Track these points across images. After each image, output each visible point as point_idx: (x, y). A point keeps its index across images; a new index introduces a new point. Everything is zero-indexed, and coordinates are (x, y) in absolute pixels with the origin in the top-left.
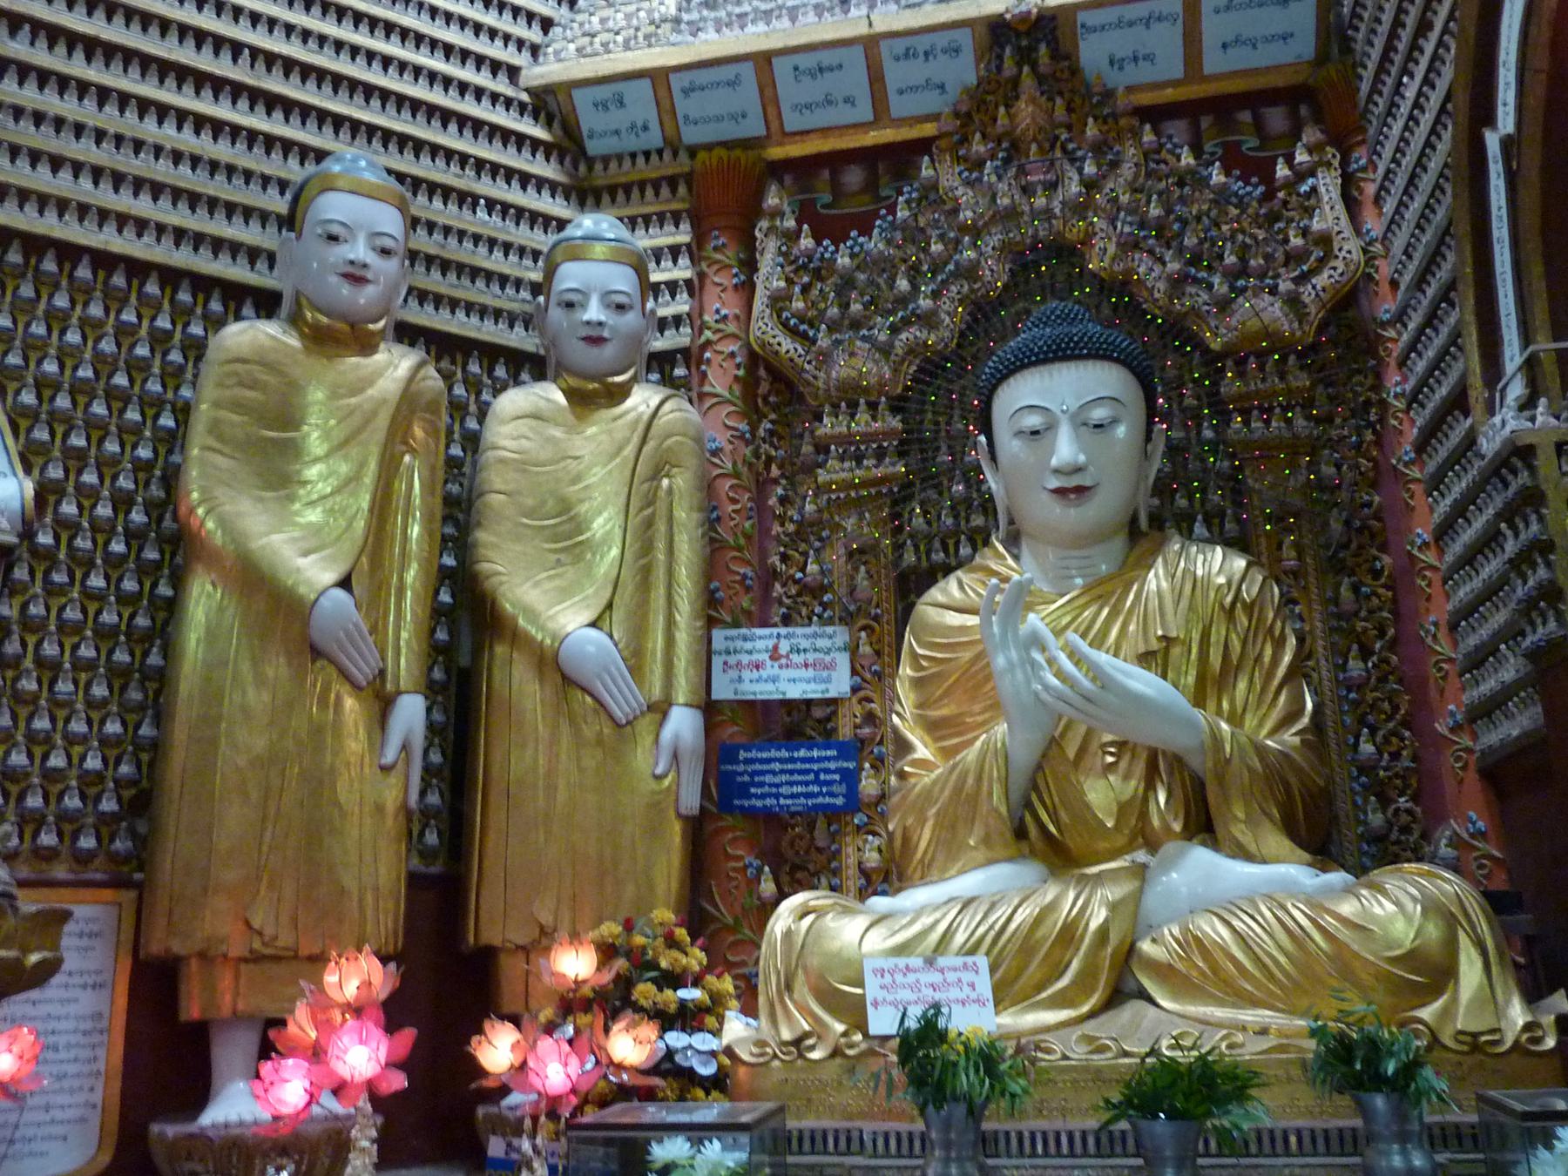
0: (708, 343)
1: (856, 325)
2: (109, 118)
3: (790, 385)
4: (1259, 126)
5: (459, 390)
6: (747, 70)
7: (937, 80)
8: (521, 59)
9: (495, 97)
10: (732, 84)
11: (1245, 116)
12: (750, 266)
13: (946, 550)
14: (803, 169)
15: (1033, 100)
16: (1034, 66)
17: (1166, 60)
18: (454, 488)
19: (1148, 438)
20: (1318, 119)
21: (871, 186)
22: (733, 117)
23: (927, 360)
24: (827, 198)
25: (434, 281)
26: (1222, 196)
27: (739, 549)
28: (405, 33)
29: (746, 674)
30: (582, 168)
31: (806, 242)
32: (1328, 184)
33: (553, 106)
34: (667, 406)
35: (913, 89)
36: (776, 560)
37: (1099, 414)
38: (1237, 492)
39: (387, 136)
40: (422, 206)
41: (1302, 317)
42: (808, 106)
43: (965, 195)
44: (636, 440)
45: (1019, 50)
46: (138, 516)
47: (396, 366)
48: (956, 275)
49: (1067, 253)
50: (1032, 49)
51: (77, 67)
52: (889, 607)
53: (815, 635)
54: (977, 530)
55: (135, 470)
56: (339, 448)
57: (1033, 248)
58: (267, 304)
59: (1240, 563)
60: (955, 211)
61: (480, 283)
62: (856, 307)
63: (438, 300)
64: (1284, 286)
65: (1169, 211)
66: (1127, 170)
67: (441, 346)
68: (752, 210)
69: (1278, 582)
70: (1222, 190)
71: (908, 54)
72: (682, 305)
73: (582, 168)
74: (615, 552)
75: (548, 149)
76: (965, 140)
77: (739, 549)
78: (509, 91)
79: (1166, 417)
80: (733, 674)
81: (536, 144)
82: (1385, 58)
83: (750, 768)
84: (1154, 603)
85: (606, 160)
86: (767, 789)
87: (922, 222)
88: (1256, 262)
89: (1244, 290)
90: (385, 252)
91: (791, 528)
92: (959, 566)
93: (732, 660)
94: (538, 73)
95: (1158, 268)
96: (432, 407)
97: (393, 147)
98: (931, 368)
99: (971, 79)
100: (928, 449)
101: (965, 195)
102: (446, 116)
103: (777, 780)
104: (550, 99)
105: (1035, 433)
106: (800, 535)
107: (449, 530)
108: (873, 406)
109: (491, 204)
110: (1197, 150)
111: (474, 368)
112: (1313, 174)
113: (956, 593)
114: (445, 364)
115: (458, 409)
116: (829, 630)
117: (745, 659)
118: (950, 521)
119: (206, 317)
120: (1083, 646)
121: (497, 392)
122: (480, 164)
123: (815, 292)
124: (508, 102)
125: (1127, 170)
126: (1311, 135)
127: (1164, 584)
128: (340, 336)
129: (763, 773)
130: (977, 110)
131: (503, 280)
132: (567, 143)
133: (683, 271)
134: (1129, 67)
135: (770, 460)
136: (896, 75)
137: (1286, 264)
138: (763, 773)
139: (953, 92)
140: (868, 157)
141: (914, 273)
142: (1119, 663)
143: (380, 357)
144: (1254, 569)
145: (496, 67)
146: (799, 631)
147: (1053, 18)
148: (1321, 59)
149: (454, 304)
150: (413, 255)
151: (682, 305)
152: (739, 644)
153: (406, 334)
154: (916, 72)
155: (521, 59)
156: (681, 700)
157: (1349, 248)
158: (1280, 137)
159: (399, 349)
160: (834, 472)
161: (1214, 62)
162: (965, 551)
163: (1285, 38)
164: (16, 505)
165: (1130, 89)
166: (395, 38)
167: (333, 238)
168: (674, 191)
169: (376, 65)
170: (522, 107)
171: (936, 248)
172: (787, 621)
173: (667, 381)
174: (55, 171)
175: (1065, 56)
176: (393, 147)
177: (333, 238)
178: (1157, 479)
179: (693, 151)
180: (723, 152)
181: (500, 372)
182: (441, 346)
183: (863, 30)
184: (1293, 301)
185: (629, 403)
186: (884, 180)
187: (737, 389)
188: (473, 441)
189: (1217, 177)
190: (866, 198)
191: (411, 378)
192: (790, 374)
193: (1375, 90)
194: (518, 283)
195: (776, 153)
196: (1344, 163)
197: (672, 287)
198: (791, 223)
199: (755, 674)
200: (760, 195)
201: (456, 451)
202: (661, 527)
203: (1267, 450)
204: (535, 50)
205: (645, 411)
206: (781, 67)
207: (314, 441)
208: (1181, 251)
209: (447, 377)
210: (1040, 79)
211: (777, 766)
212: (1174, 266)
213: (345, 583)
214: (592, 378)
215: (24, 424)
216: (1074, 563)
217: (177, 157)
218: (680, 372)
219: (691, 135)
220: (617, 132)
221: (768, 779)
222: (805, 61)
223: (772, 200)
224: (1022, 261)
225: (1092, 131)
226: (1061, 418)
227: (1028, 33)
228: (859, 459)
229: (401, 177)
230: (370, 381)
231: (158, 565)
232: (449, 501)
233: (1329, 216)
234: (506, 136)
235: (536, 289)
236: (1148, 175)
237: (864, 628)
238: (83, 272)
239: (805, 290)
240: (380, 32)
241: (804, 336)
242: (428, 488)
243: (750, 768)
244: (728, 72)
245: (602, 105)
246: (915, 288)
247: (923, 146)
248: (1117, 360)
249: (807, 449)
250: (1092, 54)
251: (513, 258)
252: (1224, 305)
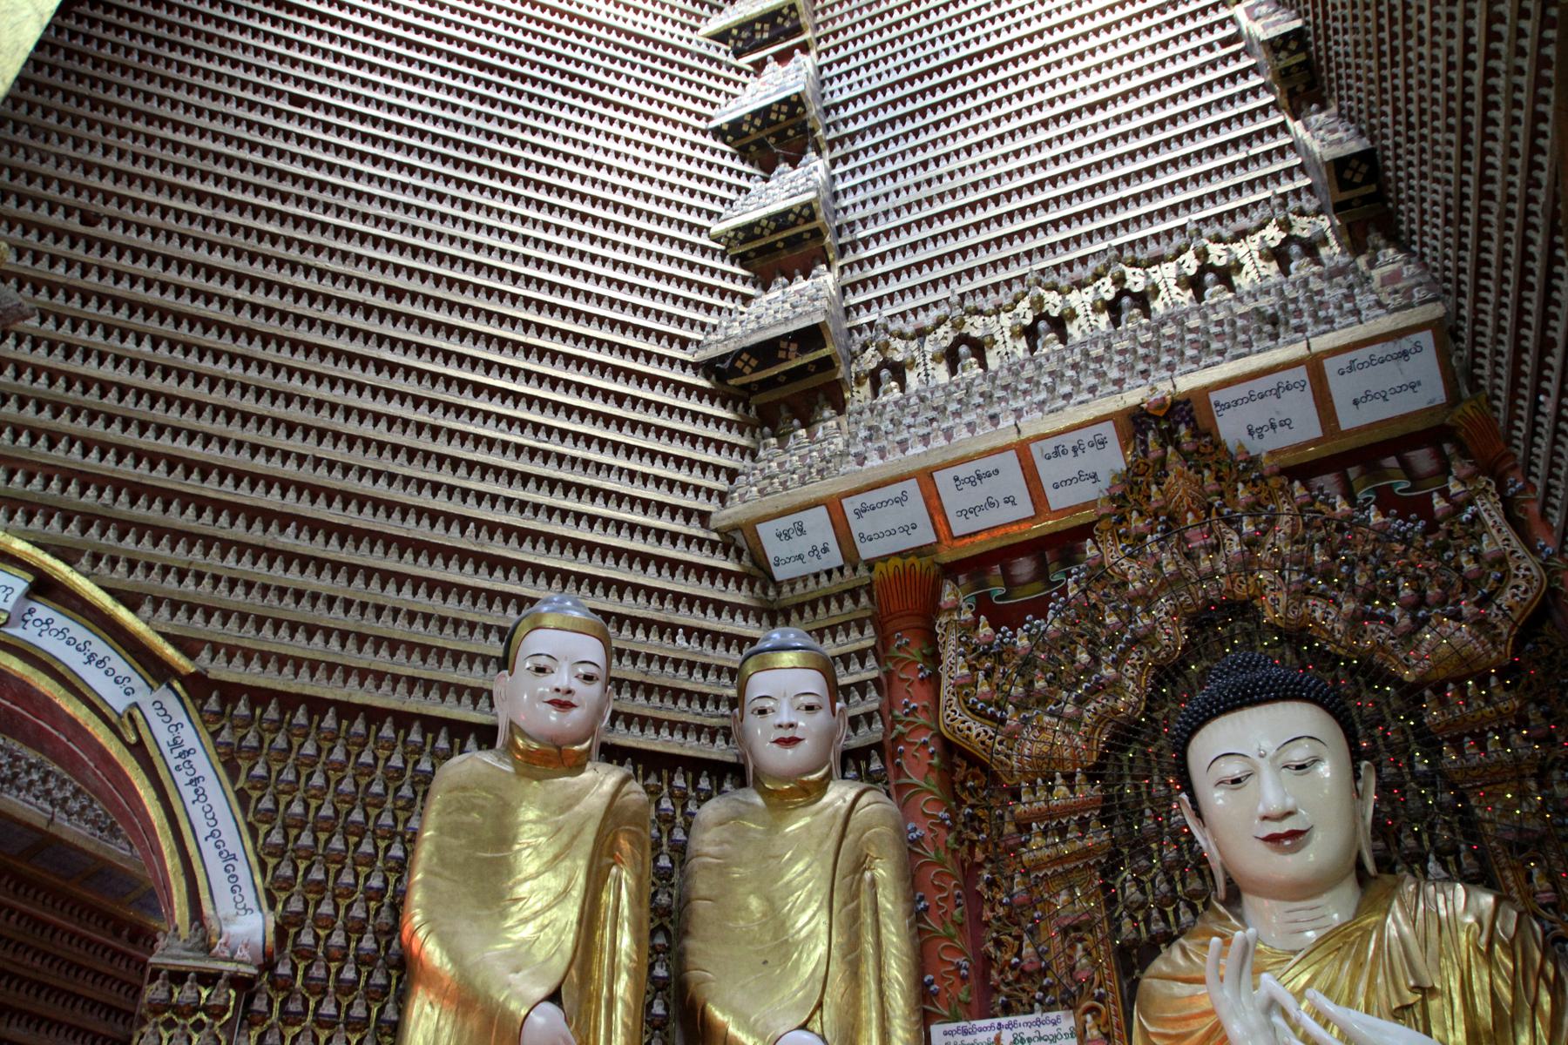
0: (901, 736)
1: (1042, 701)
2: (357, 589)
3: (985, 767)
4: (1407, 468)
5: (666, 804)
6: (912, 486)
8: (712, 506)
9: (689, 539)
11: (1391, 462)
12: (935, 658)
13: (1165, 918)
14: (974, 567)
15: (1181, 475)
16: (1177, 445)
17: (1305, 427)
18: (663, 899)
19: (1356, 776)
20: (1463, 452)
21: (1041, 574)
22: (905, 530)
23: (1119, 726)
24: (999, 590)
25: (639, 705)
26: (1384, 536)
27: (950, 938)
28: (608, 495)
30: (771, 593)
31: (985, 630)
32: (1489, 509)
33: (741, 542)
34: (864, 800)
36: (990, 946)
37: (1299, 754)
38: (1469, 826)
39: (594, 581)
40: (625, 638)
41: (1495, 640)
42: (972, 511)
43: (1132, 569)
44: (834, 836)
45: (1161, 433)
46: (368, 943)
47: (601, 781)
48: (1136, 641)
49: (1244, 609)
50: (1172, 431)
51: (333, 551)
52: (1112, 986)
53: (1039, 1023)
54: (1195, 895)
55: (368, 899)
56: (552, 864)
57: (1206, 609)
58: (486, 736)
59: (1487, 900)
60: (1125, 584)
61: (682, 704)
62: (1040, 684)
63: (643, 722)
64: (1467, 609)
65: (1334, 557)
66: (1284, 524)
67: (648, 763)
68: (931, 608)
69: (1538, 918)
70: (1382, 530)
71: (1058, 452)
72: (873, 701)
73: (771, 593)
74: (822, 949)
75: (739, 578)
76: (1122, 519)
77: (950, 938)
78: (701, 534)
79: (1370, 755)
81: (727, 575)
82: (1515, 384)
84: (1397, 951)
85: (792, 582)
87: (1093, 597)
88: (1433, 592)
89: (1426, 620)
90: (588, 678)
91: (1001, 911)
92: (1182, 933)
94: (723, 516)
95: (1333, 610)
96: (637, 819)
97: (599, 591)
98: (1125, 733)
99: (1120, 466)
100: (1132, 812)
101: (1132, 569)
102: (645, 559)
104: (738, 536)
105: (1236, 781)
106: (1012, 918)
107: (660, 940)
108: (1069, 778)
109: (689, 632)
110: (1350, 497)
111: (679, 782)
112: (1471, 502)
113: (1181, 961)
114: (652, 780)
115: (667, 820)
116: (1053, 1015)
118: (1164, 887)
119: (433, 753)
120: (1329, 1006)
121: (701, 802)
122: (677, 598)
123: (997, 676)
124: (701, 542)
125: (1284, 524)
126: (1459, 467)
127: (1406, 929)
128: (555, 758)
130: (1129, 491)
131: (703, 698)
132: (758, 572)
133: (871, 671)
134: (1268, 434)
135: (973, 844)
136: (1048, 472)
137: (1465, 589)
139: (1105, 481)
140: (1034, 547)
141: (1093, 646)
142: (1372, 1020)
143: (587, 776)
144: (1503, 906)
145: (688, 514)
146: (1021, 1019)
148: (1453, 397)
149: (658, 724)
150: (618, 683)
151: (873, 701)
153: (612, 754)
154: (1067, 466)
155: (712, 506)
157: (1526, 566)
158: (1432, 474)
159: (604, 767)
160: (1038, 847)
161: (1349, 418)
162: (1186, 917)
163: (1413, 386)
164: (258, 939)
165: (1272, 453)
166: (599, 500)
167: (540, 670)
168: (856, 601)
169: (583, 523)
170: (714, 546)
171: (1111, 620)
172: (1007, 1010)
173: (871, 779)
174: (310, 638)
175: (1206, 433)
176: (599, 591)
177: (540, 670)
178: (1375, 821)
179: (870, 565)
180: (898, 561)
181: (704, 784)
182: (648, 763)
183: (1013, 438)
184: (1481, 624)
185: (826, 799)
186: (1053, 567)
187: (933, 778)
188: (681, 851)
189: (1375, 517)
190: (1038, 585)
191: (615, 794)
192: (985, 757)
193: (1512, 416)
194: (717, 700)
195: (946, 556)
196: (1501, 488)
197: (861, 687)
198: (968, 616)
200: (937, 594)
201: (664, 862)
202: (867, 918)
203: (1492, 777)
204: (723, 497)
205: (843, 806)
206: (943, 479)
207: (528, 863)
208: (1353, 590)
209: (654, 793)
210: (1186, 457)
212: (1349, 606)
213: (554, 997)
214: (786, 779)
215: (271, 862)
216: (1303, 915)
217: (412, 616)
218: (876, 765)
219: (867, 551)
222: (964, 471)
223: (948, 596)
224: (1201, 621)
225: (1243, 493)
226: (1267, 771)
227: (1166, 418)
228: (1062, 831)
229: (606, 616)
230: (576, 799)
231: (385, 990)
232: (658, 911)
233: (1497, 538)
234: (700, 570)
235: (734, 703)
236: (1306, 526)
237: (1089, 1010)
238: (329, 722)
239: (988, 674)
240: (586, 496)
241: (992, 717)
242: (636, 901)
244: (895, 490)
245: (785, 535)
246: (1096, 660)
247: (1085, 531)
248: (1308, 699)
249: (1009, 828)
250: (1231, 428)
251: (711, 677)
252: (1409, 637)
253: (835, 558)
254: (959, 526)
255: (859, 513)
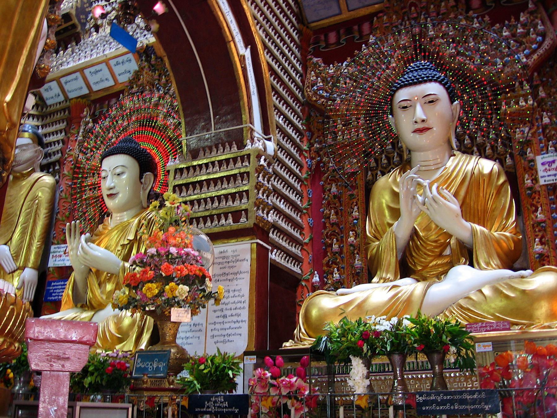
7: (127, 70)
10: (76, 79)
29: (58, 259)
35: (122, 73)
37: (118, 171)
71: (118, 64)
80: (54, 259)
83: (54, 288)
85: (50, 106)
86: (56, 294)
93: (55, 254)
103: (59, 291)
117: (58, 254)
129: (56, 289)
133: (60, 136)
138: (56, 289)
147: (152, 47)
152: (57, 250)
156: (30, 266)
180: (75, 100)
195: (93, 98)
199: (59, 259)
206: (87, 72)
211: (60, 287)
220: (52, 97)
221: (57, 291)
222: (93, 69)
243: (54, 288)
244: (73, 76)
253: (62, 98)
254: (95, 88)
255: (66, 83)
